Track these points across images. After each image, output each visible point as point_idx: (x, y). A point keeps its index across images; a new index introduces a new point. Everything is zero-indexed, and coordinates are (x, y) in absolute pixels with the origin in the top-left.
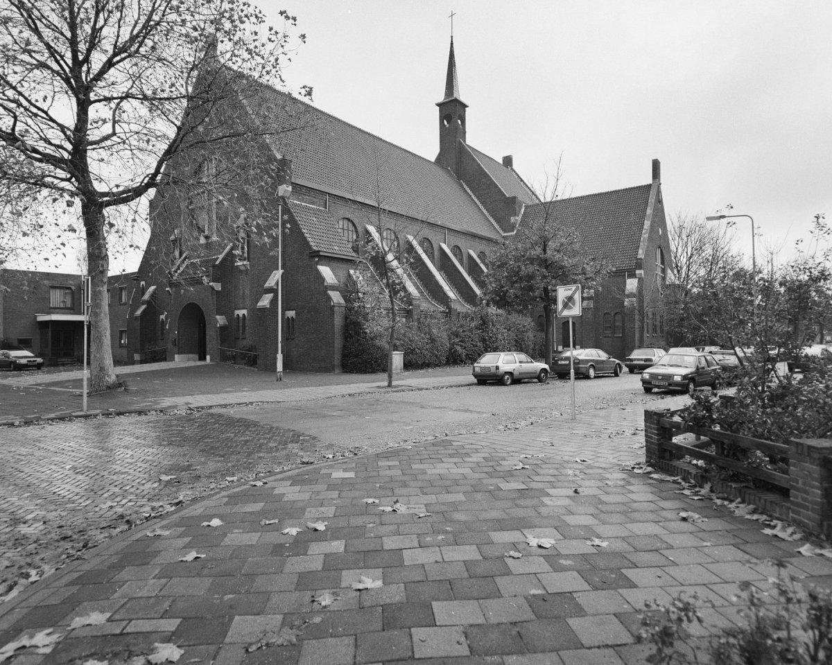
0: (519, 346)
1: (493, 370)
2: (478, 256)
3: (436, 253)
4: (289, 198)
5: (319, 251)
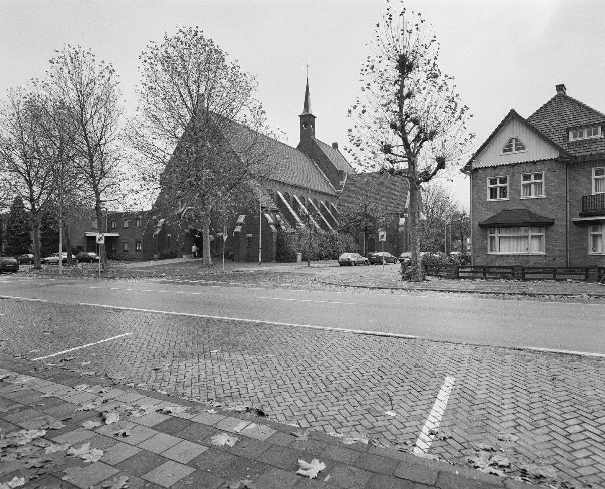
0: (359, 251)
1: (347, 260)
2: (313, 201)
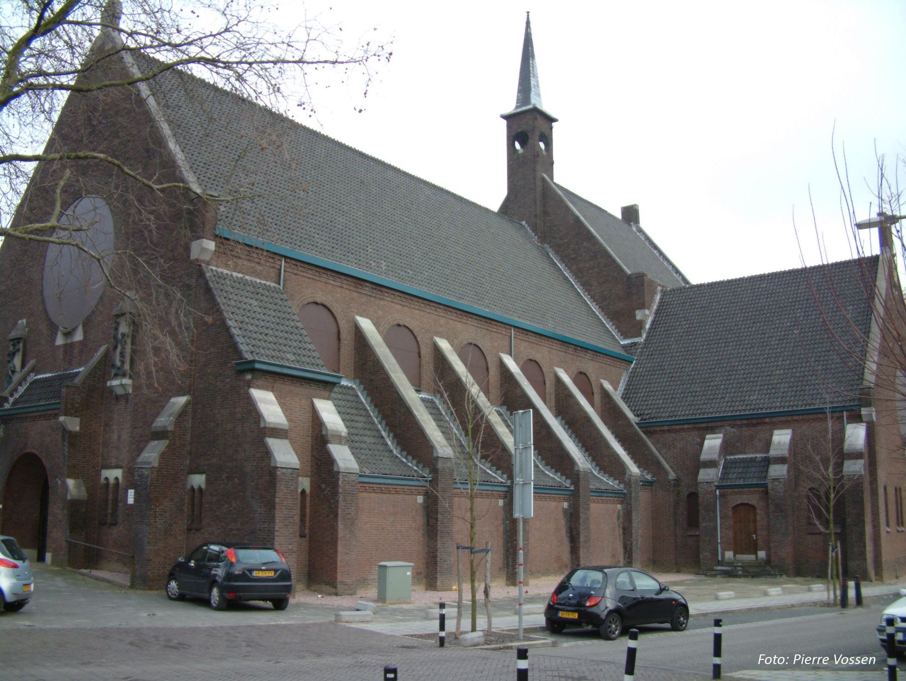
2: (575, 381)
3: (596, 390)
4: (208, 264)
5: (254, 361)
